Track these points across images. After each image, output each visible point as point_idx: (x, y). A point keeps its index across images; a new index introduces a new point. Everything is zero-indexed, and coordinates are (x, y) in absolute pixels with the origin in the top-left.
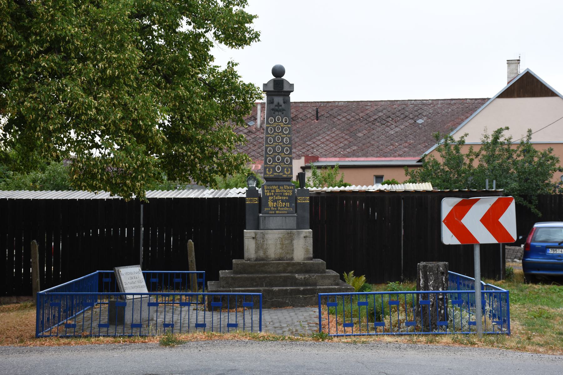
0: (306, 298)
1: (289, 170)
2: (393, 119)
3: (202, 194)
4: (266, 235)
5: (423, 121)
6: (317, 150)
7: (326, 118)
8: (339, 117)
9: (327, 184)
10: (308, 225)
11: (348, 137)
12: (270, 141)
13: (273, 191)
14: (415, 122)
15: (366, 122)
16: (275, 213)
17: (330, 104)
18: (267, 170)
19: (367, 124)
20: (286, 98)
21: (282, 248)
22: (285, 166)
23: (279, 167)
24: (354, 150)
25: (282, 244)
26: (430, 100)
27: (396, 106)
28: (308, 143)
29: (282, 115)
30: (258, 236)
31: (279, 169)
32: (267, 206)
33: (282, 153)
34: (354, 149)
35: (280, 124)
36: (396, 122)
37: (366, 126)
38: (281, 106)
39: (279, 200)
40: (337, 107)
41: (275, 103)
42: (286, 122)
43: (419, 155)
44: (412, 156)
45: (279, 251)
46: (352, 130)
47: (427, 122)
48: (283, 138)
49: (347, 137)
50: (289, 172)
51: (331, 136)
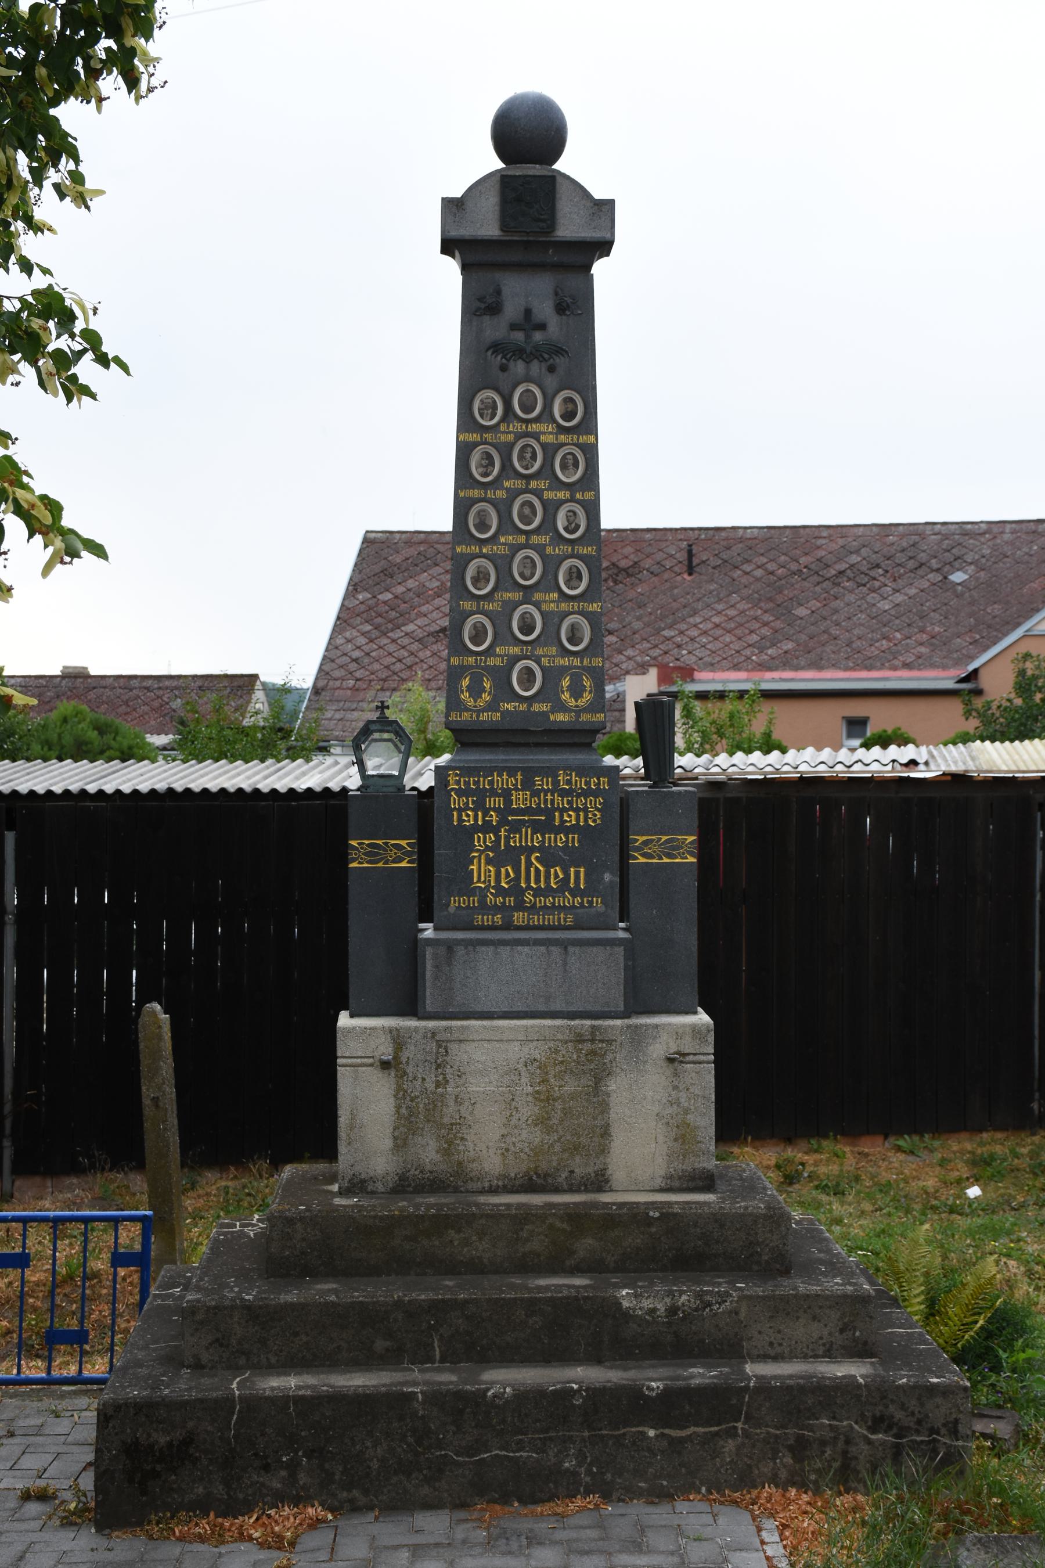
0: (681, 1441)
1: (587, 683)
2: (887, 572)
3: (344, 774)
4: (453, 1047)
5: (966, 577)
6: (690, 653)
7: (714, 568)
8: (747, 568)
9: (724, 741)
10: (690, 989)
11: (771, 618)
12: (483, 526)
13: (498, 802)
14: (946, 578)
15: (816, 578)
16: (508, 926)
17: (723, 534)
18: (465, 682)
19: (818, 583)
20: (572, 281)
21: (542, 1122)
22: (565, 662)
23: (529, 671)
24: (786, 652)
25: (545, 1099)
26: (982, 522)
27: (895, 539)
28: (667, 633)
29: (551, 381)
30: (409, 1052)
31: (528, 677)
32: (464, 883)
33: (549, 590)
34: (785, 648)
35: (534, 427)
36: (895, 580)
37: (818, 589)
38: (542, 327)
39: (530, 850)
40: (741, 540)
41: (512, 310)
42: (569, 416)
43: (958, 663)
44: (938, 667)
45: (530, 1136)
46: (779, 599)
47: (977, 579)
48: (551, 509)
49: (767, 618)
50: (587, 697)
51: (726, 615)
